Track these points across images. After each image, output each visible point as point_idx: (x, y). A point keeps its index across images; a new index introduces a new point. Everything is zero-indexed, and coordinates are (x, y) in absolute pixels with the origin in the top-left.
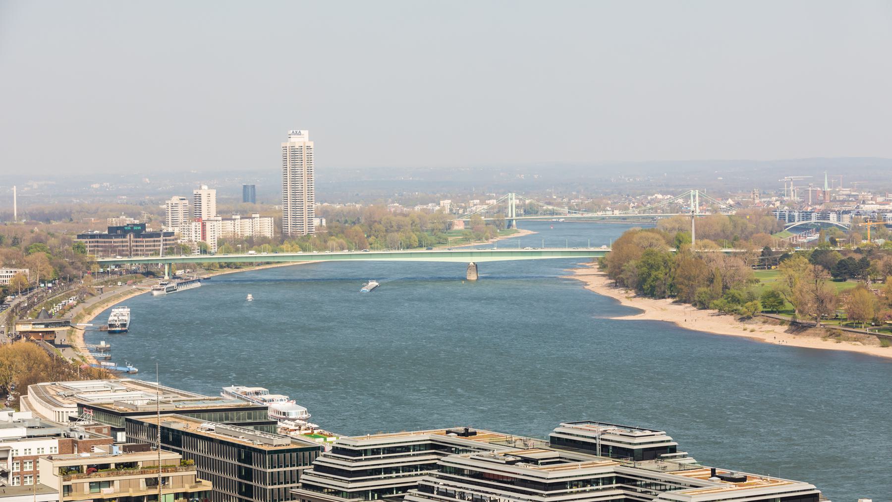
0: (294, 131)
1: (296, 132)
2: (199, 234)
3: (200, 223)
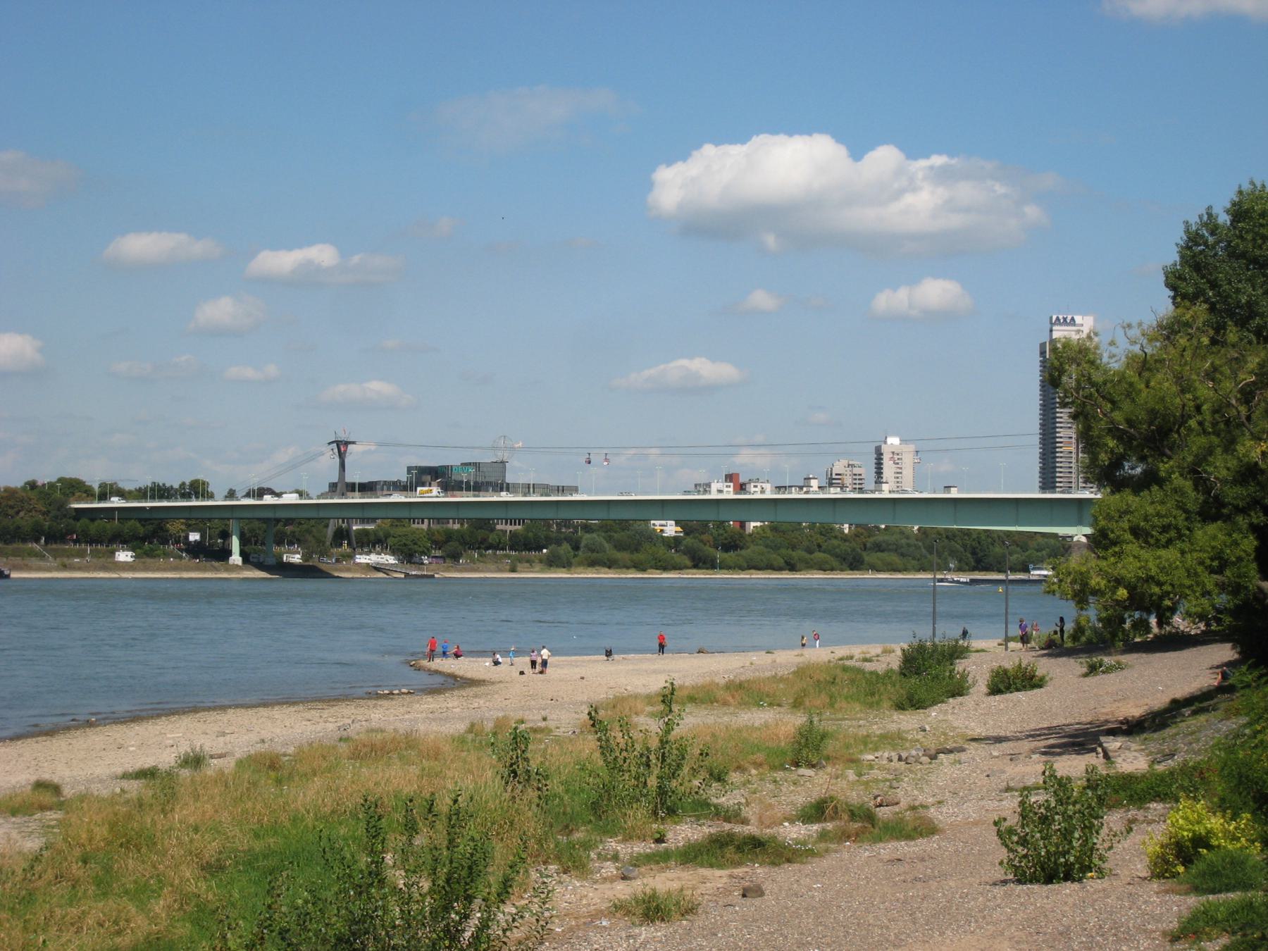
0: (1061, 317)
1: (1065, 319)
2: (763, 491)
3: (732, 484)
